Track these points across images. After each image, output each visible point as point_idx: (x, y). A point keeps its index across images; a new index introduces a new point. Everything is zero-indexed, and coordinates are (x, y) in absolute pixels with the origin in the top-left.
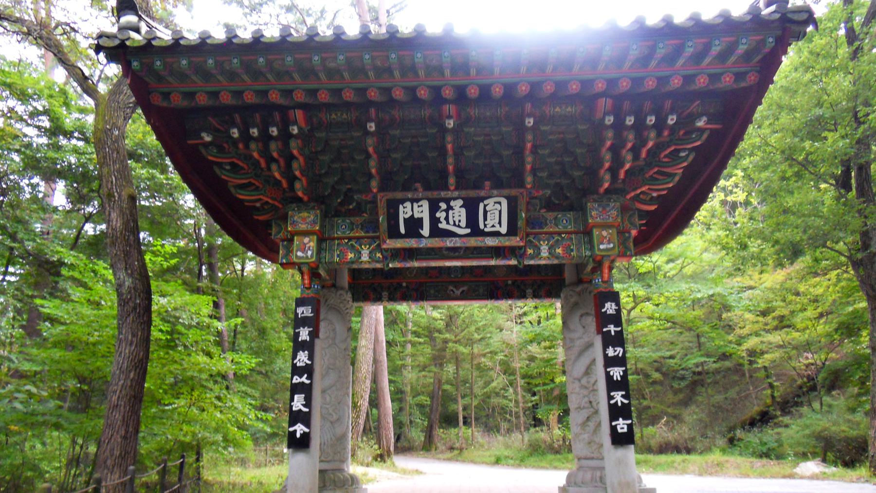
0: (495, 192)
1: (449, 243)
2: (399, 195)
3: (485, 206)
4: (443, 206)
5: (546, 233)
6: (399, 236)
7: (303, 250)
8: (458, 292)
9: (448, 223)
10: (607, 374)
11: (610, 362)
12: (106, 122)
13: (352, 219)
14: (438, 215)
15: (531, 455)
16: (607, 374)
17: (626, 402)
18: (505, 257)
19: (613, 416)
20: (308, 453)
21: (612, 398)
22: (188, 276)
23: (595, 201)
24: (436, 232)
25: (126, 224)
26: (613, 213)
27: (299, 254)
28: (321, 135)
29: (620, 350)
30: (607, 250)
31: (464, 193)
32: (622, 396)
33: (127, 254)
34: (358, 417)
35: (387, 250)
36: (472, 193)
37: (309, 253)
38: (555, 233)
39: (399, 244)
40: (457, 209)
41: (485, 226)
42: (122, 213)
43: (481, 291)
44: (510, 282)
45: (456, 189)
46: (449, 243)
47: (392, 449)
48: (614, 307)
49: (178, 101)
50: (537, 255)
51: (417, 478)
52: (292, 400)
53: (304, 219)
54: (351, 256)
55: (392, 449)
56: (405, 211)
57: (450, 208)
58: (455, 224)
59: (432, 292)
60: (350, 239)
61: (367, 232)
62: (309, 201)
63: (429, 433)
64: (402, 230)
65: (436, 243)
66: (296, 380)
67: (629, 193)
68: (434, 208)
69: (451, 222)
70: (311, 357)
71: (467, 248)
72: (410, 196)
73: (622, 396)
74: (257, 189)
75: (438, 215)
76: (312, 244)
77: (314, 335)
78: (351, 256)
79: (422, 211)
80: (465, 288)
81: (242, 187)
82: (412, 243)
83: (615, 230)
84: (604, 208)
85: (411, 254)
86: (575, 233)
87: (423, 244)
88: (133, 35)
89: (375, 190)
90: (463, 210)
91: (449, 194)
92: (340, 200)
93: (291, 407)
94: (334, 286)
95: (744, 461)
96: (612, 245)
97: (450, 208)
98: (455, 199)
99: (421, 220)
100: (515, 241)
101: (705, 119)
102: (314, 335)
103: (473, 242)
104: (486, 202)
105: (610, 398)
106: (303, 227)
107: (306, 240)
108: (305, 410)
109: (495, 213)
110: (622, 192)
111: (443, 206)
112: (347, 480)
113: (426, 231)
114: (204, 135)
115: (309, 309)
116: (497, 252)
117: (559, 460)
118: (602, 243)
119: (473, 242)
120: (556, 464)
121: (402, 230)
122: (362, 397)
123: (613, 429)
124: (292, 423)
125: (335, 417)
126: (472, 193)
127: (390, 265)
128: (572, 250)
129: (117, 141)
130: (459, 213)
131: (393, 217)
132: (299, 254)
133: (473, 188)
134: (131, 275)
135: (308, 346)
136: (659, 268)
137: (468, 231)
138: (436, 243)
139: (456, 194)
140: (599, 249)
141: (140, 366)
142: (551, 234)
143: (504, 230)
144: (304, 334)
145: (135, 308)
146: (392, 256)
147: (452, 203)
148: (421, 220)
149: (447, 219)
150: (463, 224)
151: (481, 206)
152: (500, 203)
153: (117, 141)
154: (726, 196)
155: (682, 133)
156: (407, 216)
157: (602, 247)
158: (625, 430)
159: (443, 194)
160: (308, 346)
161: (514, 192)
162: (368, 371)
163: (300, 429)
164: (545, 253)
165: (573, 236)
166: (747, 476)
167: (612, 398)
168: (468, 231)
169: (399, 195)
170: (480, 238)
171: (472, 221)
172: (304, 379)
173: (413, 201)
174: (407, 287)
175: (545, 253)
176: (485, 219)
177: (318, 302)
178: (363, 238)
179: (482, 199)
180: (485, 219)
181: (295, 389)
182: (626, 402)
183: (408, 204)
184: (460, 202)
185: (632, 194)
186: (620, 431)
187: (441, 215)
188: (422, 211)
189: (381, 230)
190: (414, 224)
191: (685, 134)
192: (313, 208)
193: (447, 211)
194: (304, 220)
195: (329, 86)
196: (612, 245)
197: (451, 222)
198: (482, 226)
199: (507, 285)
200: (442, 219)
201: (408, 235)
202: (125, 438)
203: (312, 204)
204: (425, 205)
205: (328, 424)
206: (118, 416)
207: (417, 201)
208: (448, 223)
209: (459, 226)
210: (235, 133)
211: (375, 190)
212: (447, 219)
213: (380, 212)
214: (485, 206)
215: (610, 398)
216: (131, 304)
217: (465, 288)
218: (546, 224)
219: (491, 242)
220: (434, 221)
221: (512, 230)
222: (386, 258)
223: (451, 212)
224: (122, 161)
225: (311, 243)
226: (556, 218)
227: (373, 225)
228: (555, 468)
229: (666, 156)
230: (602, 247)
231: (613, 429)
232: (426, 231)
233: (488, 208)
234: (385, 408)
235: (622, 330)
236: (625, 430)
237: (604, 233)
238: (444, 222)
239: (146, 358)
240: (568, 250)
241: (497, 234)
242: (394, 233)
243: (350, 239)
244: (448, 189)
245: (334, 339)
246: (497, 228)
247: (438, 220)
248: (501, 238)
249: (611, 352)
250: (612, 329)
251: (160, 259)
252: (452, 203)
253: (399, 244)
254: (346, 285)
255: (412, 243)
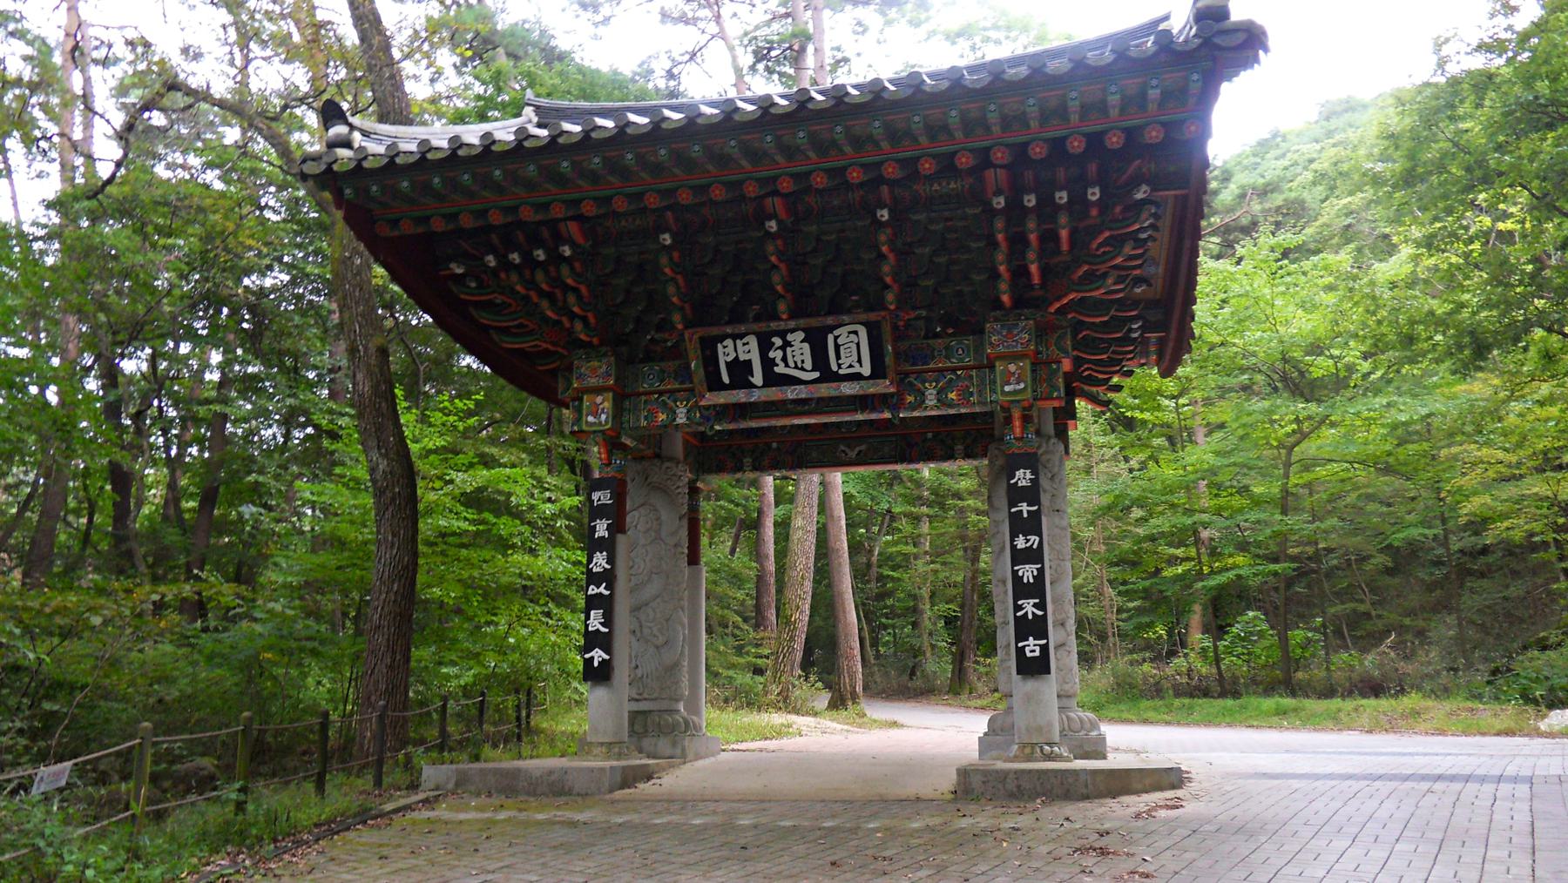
0: (846, 318)
1: (791, 393)
2: (715, 331)
3: (836, 338)
4: (778, 341)
5: (933, 371)
6: (722, 387)
7: (596, 414)
8: (853, 454)
9: (787, 365)
10: (1015, 573)
11: (1019, 557)
12: (344, 248)
13: (663, 364)
14: (771, 354)
15: (1117, 701)
16: (1015, 573)
17: (1040, 613)
18: (873, 410)
19: (1021, 636)
20: (610, 686)
21: (1020, 608)
22: (96, 577)
23: (996, 320)
24: (772, 379)
25: (375, 387)
26: (1023, 337)
27: (590, 419)
28: (609, 251)
29: (1034, 539)
30: (1015, 392)
31: (802, 322)
32: (1035, 605)
33: (379, 429)
34: (792, 639)
35: (708, 408)
36: (814, 322)
37: (603, 417)
38: (947, 369)
39: (722, 398)
40: (797, 344)
41: (839, 366)
42: (370, 373)
43: (886, 449)
44: (930, 435)
45: (791, 318)
46: (791, 393)
47: (859, 689)
48: (1029, 476)
49: (407, 228)
50: (920, 404)
51: (894, 734)
52: (588, 618)
53: (594, 370)
54: (662, 417)
55: (859, 689)
56: (726, 352)
57: (787, 344)
58: (796, 367)
59: (814, 454)
60: (661, 393)
61: (682, 383)
62: (601, 345)
63: (959, 660)
64: (726, 379)
65: (773, 394)
66: (593, 590)
67: (1051, 304)
68: (765, 347)
69: (792, 364)
70: (610, 560)
71: (820, 399)
72: (729, 330)
73: (1035, 605)
74: (531, 333)
75: (771, 354)
76: (606, 404)
77: (617, 527)
78: (662, 417)
79: (749, 350)
80: (863, 447)
81: (505, 331)
82: (740, 396)
83: (1028, 362)
84: (1010, 331)
85: (743, 410)
86: (977, 368)
87: (756, 396)
88: (343, 153)
89: (680, 327)
90: (806, 346)
91: (782, 325)
92: (636, 346)
93: (587, 626)
94: (658, 456)
95: (1509, 712)
96: (1022, 386)
97: (787, 344)
98: (793, 331)
99: (749, 363)
100: (884, 386)
101: (1144, 188)
102: (617, 527)
103: (825, 390)
104: (836, 333)
105: (1018, 608)
106: (593, 381)
107: (599, 399)
108: (603, 630)
109: (852, 348)
110: (1039, 304)
111: (778, 341)
112: (678, 723)
113: (757, 379)
114: (453, 265)
115: (608, 493)
116: (863, 402)
117: (1155, 709)
118: (1008, 383)
119: (825, 390)
120: (1151, 714)
121: (726, 379)
122: (798, 607)
123: (1020, 652)
124: (588, 648)
125: (661, 640)
126: (814, 322)
127: (717, 428)
128: (972, 394)
129: (359, 273)
130: (801, 351)
131: (711, 361)
132: (590, 419)
133: (817, 308)
134: (386, 456)
135: (608, 545)
136: (1351, 369)
137: (816, 375)
138: (773, 394)
139: (792, 324)
140: (1003, 393)
141: (407, 572)
142: (940, 370)
143: (866, 370)
144: (602, 529)
145: (393, 499)
146: (718, 413)
147: (790, 337)
148: (749, 363)
149: (784, 359)
150: (808, 365)
151: (830, 338)
152: (856, 333)
153: (359, 273)
154: (1495, 221)
155: (1118, 209)
156: (729, 359)
157: (1007, 388)
158: (1037, 654)
159: (773, 325)
160: (608, 545)
161: (873, 316)
162: (807, 568)
163: (598, 655)
164: (931, 400)
165: (974, 373)
166: (1441, 732)
167: (1020, 608)
168: (816, 375)
169: (715, 331)
170: (834, 385)
171: (820, 360)
172: (602, 590)
173: (736, 337)
174: (778, 449)
175: (931, 400)
176: (838, 357)
177: (623, 483)
178: (679, 391)
179: (832, 329)
180: (838, 357)
181: (592, 602)
182: (1040, 613)
183: (729, 342)
184: (800, 335)
185: (1057, 305)
186: (1029, 655)
187: (776, 354)
188: (749, 350)
189: (696, 380)
190: (741, 370)
191: (1123, 212)
192: (605, 355)
193: (783, 348)
194: (595, 371)
195: (592, 194)
196: (1022, 386)
197: (792, 364)
198: (834, 368)
199: (925, 440)
200: (778, 361)
201: (733, 386)
202: (391, 667)
203: (603, 349)
204: (753, 342)
205: (652, 650)
206: (381, 639)
207: (741, 336)
208: (787, 365)
209: (803, 369)
210: (491, 260)
211: (680, 327)
212: (784, 359)
213: (691, 354)
214: (836, 338)
215: (1018, 608)
216: (389, 495)
217: (863, 447)
218: (933, 357)
219: (848, 389)
220: (768, 364)
221: (878, 372)
222: (709, 420)
223: (789, 350)
224: (367, 301)
225: (605, 403)
226: (947, 348)
227: (684, 374)
228: (1146, 722)
229: (1101, 245)
230: (1007, 388)
231: (1020, 652)
232: (757, 379)
233: (840, 341)
234: (846, 625)
235: (1038, 511)
236: (1037, 654)
237: (1012, 368)
238: (782, 364)
239: (413, 568)
240: (965, 394)
241: (857, 377)
242: (715, 384)
243: (661, 393)
244: (780, 319)
245: (658, 532)
246: (857, 369)
247: (773, 362)
248: (862, 383)
249: (1021, 543)
250: (1024, 508)
251: (452, 419)
252: (790, 337)
253: (722, 398)
254: (681, 456)
255: (740, 396)
